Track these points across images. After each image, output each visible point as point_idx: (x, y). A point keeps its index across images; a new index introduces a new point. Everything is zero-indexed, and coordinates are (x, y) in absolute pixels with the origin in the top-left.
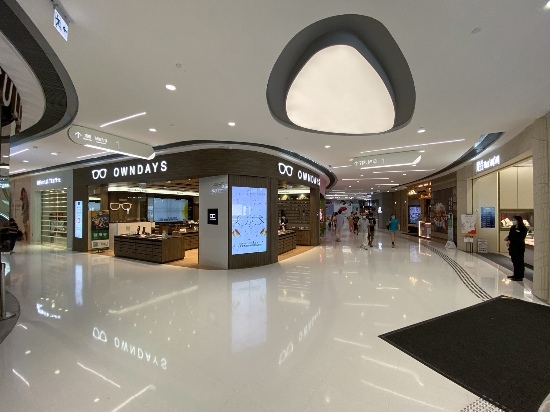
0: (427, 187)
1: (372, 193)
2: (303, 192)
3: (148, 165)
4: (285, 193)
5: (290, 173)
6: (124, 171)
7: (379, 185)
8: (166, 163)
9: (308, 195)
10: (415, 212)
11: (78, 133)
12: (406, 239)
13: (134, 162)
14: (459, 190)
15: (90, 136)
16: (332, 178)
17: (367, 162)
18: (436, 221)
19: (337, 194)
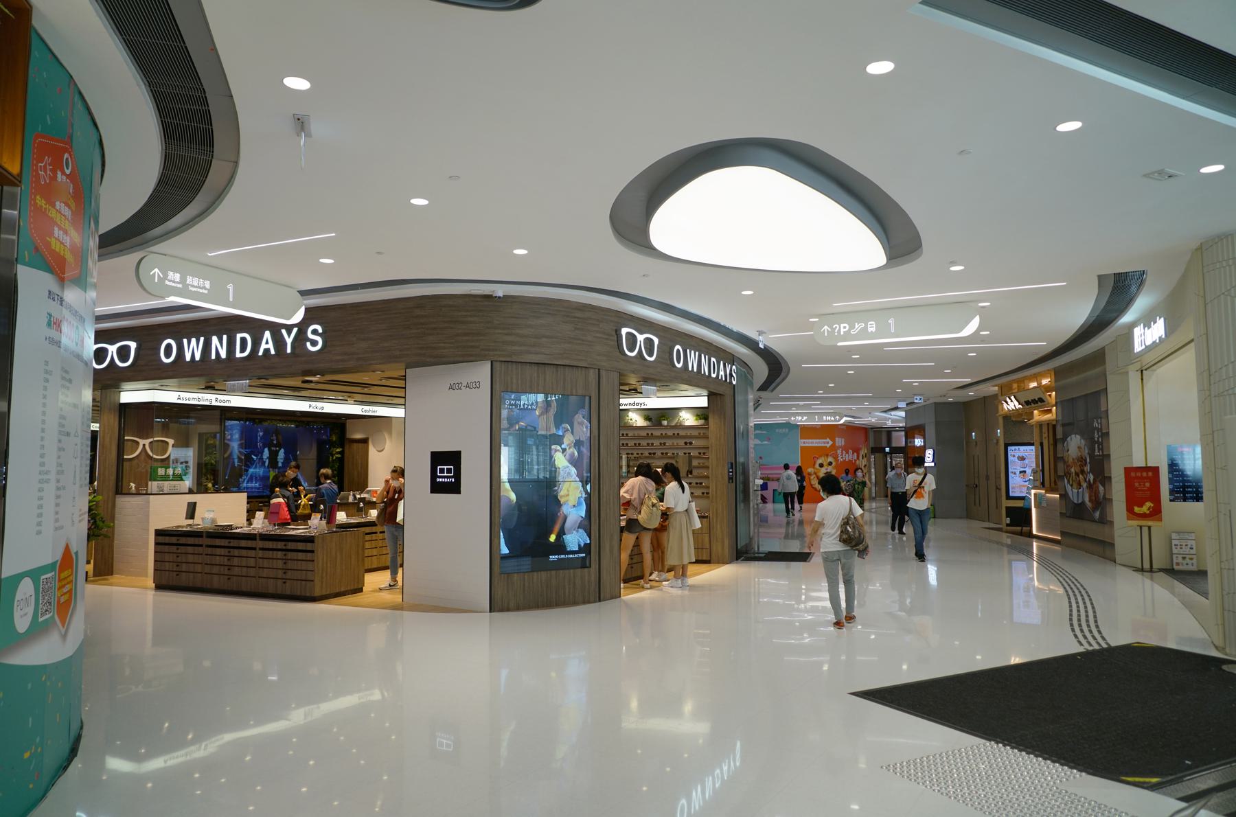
0: (1048, 389)
1: (902, 405)
2: (687, 403)
3: (267, 334)
4: (635, 408)
5: (650, 354)
6: (193, 349)
7: (916, 382)
8: (320, 331)
9: (702, 413)
10: (1022, 464)
11: (156, 270)
12: (1002, 544)
13: (228, 325)
14: (1113, 398)
15: (177, 277)
16: (776, 366)
17: (852, 327)
18: (1069, 488)
19: (797, 406)
